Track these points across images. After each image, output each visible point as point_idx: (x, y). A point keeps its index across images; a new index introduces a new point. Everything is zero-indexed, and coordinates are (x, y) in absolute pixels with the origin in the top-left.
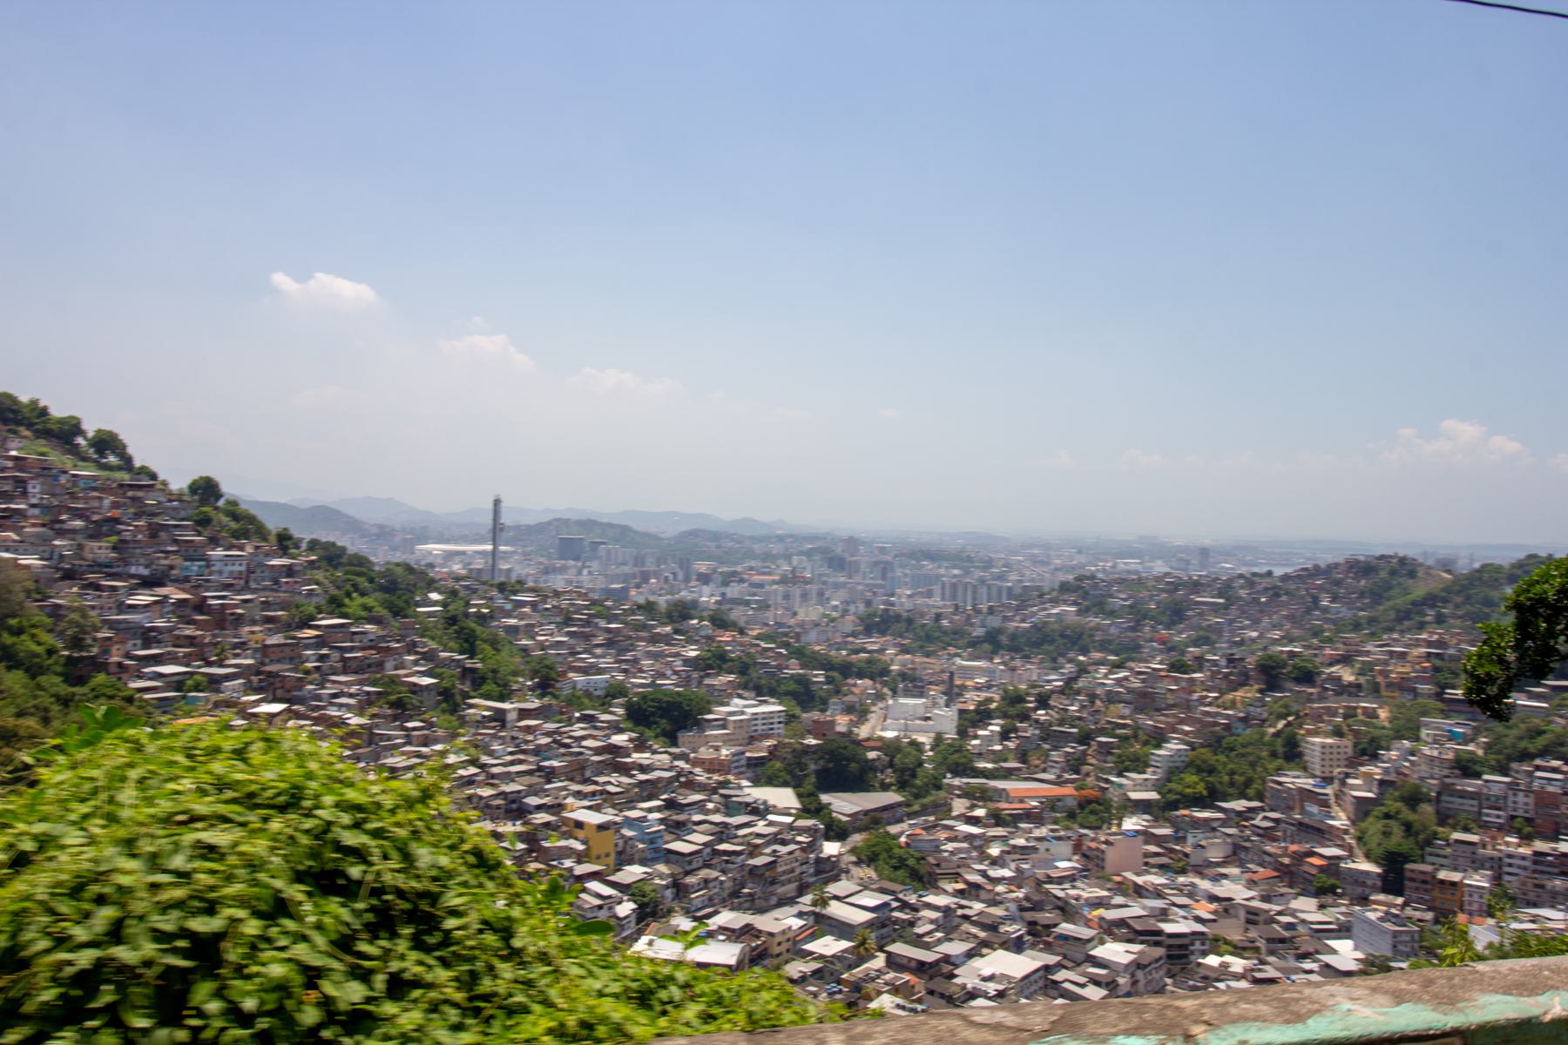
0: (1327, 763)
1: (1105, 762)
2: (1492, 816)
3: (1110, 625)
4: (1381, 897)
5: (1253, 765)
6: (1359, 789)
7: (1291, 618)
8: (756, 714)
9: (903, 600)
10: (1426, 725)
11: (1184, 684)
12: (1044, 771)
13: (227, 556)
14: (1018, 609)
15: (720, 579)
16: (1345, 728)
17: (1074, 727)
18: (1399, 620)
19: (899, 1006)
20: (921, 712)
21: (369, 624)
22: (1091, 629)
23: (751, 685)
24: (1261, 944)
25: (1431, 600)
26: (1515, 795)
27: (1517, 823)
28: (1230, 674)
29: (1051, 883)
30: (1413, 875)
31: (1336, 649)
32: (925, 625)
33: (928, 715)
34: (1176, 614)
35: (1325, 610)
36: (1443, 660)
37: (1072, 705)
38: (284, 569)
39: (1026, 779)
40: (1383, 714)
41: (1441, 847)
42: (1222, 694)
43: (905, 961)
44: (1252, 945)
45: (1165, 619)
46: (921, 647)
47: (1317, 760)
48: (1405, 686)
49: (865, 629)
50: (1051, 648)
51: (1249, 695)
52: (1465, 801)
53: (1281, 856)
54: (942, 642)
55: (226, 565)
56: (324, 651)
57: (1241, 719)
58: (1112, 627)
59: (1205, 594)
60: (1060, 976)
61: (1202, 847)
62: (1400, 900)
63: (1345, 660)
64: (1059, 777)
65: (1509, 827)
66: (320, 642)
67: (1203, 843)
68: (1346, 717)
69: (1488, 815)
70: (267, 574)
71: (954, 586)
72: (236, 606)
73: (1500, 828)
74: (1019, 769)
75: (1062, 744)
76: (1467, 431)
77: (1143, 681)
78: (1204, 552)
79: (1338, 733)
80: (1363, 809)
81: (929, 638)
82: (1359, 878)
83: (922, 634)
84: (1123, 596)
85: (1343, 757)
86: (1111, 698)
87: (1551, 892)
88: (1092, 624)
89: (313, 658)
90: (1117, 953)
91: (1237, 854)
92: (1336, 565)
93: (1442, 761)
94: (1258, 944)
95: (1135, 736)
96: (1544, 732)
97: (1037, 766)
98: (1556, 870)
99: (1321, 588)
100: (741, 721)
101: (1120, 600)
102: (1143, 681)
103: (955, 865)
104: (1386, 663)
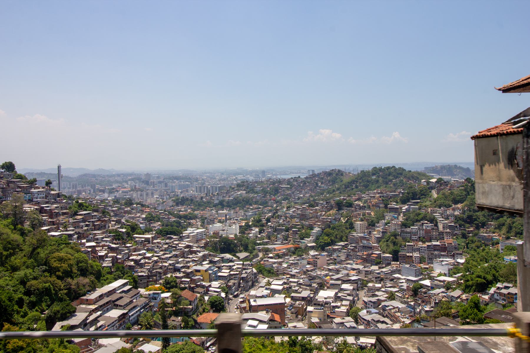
0: (362, 229)
1: (295, 236)
2: (414, 237)
3: (257, 196)
4: (393, 263)
5: (342, 232)
6: (376, 234)
7: (311, 190)
8: (198, 232)
9: (192, 192)
10: (386, 215)
11: (314, 211)
12: (276, 241)
13: (38, 191)
14: (227, 193)
15: (108, 191)
16: (364, 219)
17: (283, 227)
18: (346, 188)
19: (315, 309)
20: (221, 228)
21: (95, 212)
22: (251, 198)
23: (165, 225)
24: (373, 279)
25: (353, 182)
26: (420, 231)
27: (421, 238)
28: (327, 206)
29: (309, 272)
30: (401, 256)
31: (356, 197)
32: (198, 201)
33: (223, 229)
34: (276, 191)
35: (320, 187)
36: (384, 197)
37: (280, 220)
38: (57, 195)
39: (272, 244)
40: (372, 214)
41: (403, 247)
42: (326, 212)
43: (298, 298)
44: (371, 280)
45: (273, 193)
46: (198, 208)
47: (359, 228)
48: (376, 205)
49: (176, 204)
50: (240, 205)
51: (334, 212)
52: (407, 234)
53: (363, 256)
54: (204, 206)
55: (39, 195)
56: (87, 223)
57: (334, 219)
58: (258, 197)
59: (284, 184)
60: (339, 295)
61: (340, 256)
62: (398, 263)
63: (359, 199)
64: (282, 242)
65: (420, 239)
66: (84, 220)
67: (339, 255)
68: (363, 216)
69: (413, 237)
70: (52, 197)
71: (200, 187)
72: (54, 209)
73: (416, 240)
74: (269, 242)
75: (280, 232)
76: (327, 132)
77: (301, 211)
78: (263, 172)
79: (362, 220)
80: (379, 240)
81: (199, 205)
82: (386, 258)
83: (197, 204)
84: (260, 187)
85: (365, 227)
86: (292, 217)
87: (435, 255)
88: (251, 196)
89: (84, 226)
90: (348, 287)
91: (348, 257)
92: (320, 173)
93: (398, 224)
94: (372, 279)
95: (303, 228)
96: (420, 214)
97: (274, 240)
98: (433, 250)
99: (318, 180)
100: (194, 235)
101: (258, 188)
102: (301, 211)
103: (282, 270)
104: (370, 200)
